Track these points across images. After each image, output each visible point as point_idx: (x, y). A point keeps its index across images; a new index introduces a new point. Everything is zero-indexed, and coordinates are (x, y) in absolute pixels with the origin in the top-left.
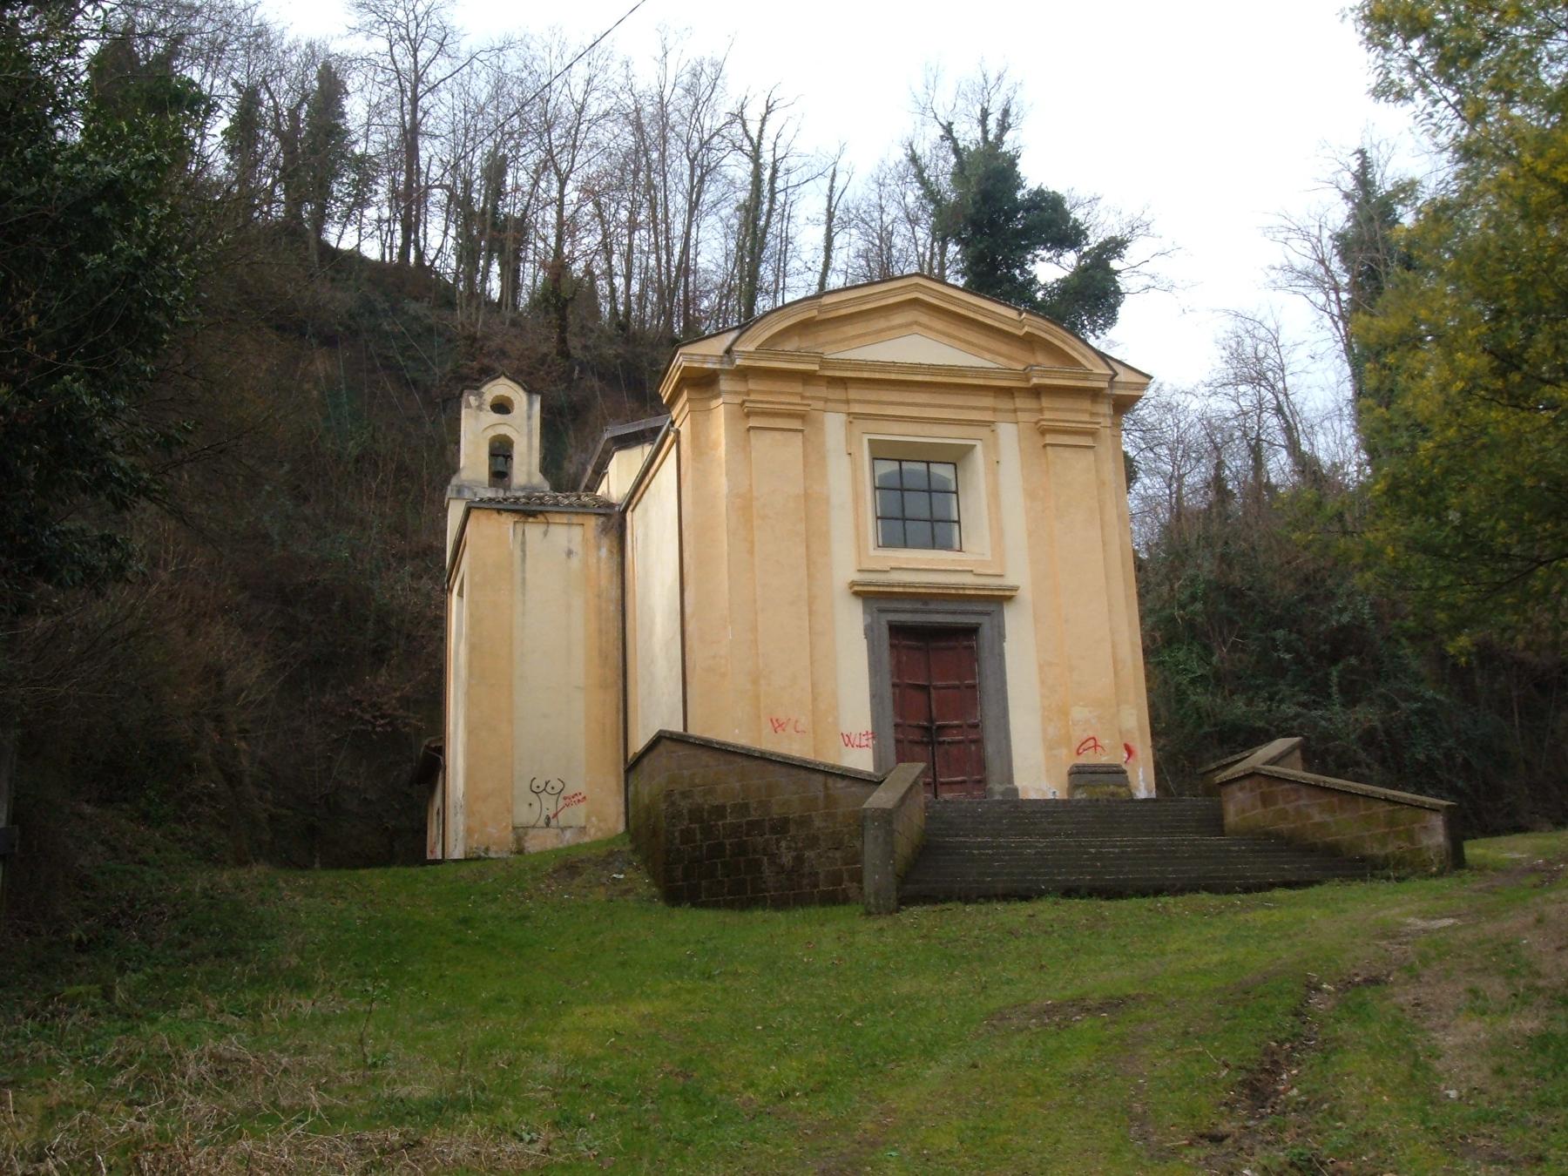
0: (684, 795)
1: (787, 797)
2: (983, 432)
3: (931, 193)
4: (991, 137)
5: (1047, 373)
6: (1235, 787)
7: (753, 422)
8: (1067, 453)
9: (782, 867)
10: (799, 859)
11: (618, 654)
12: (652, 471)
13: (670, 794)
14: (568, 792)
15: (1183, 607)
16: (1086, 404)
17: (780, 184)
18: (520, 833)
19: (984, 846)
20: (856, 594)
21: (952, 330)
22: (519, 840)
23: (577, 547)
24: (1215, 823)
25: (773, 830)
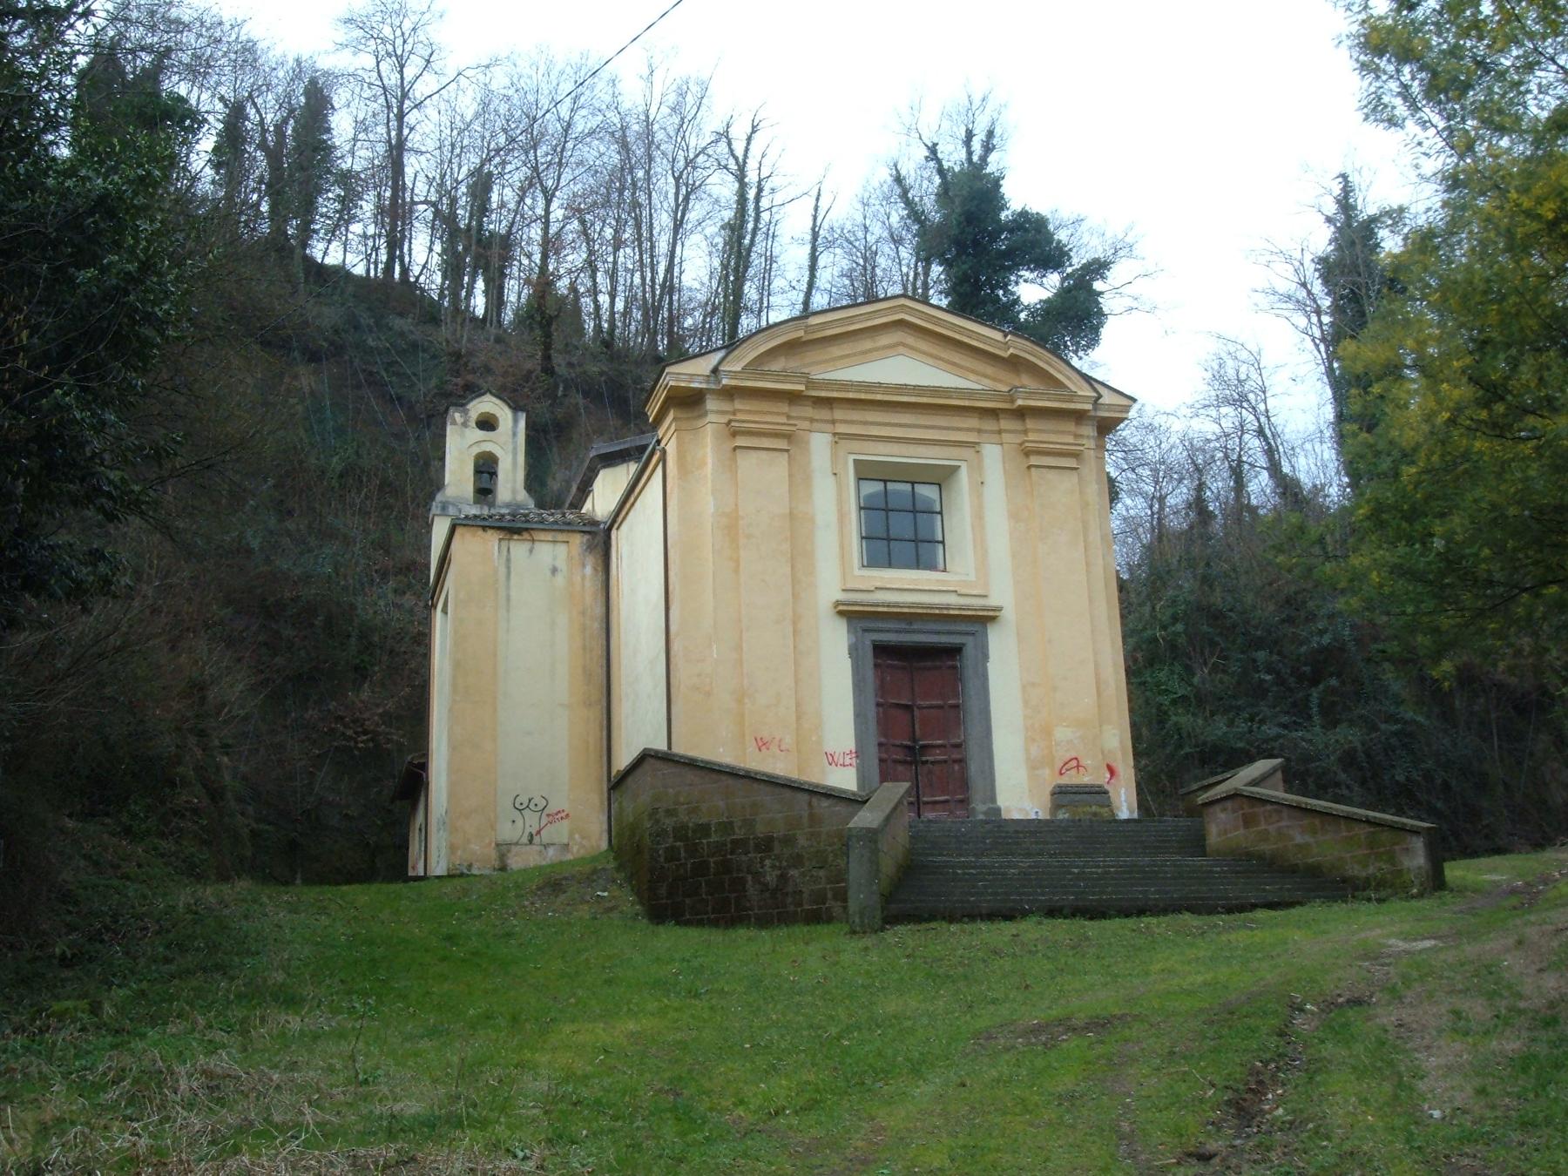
0: (670, 813)
1: (772, 816)
2: (967, 453)
3: (915, 213)
4: (975, 158)
5: (1031, 395)
6: (1217, 808)
8: (1051, 475)
9: (766, 885)
10: (783, 877)
11: (601, 672)
12: (637, 490)
13: (655, 811)
14: (551, 809)
15: (1164, 628)
16: (1070, 426)
17: (764, 203)
18: (503, 849)
19: (964, 866)
20: (841, 613)
21: (936, 350)
22: (502, 857)
23: (561, 564)
24: (1198, 844)
25: (758, 848)
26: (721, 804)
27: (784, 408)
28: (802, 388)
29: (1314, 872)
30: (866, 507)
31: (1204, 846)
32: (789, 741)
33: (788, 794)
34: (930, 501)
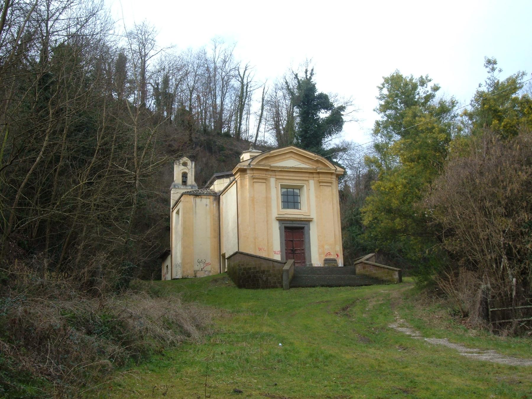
0: (242, 265)
1: (264, 266)
2: (306, 182)
3: (291, 93)
4: (308, 77)
5: (321, 169)
6: (358, 265)
7: (255, 180)
8: (326, 187)
9: (263, 280)
10: (267, 279)
11: (218, 230)
12: (228, 188)
13: (239, 265)
14: (206, 262)
15: (355, 216)
16: (330, 176)
17: (248, 90)
18: (195, 272)
19: (305, 277)
20: (277, 220)
21: (300, 158)
22: (195, 274)
23: (208, 204)
24: (354, 272)
25: (261, 273)
26: (254, 263)
27: (265, 173)
28: (269, 168)
29: (377, 279)
30: (283, 195)
31: (355, 273)
32: (266, 248)
33: (268, 261)
34: (297, 193)
